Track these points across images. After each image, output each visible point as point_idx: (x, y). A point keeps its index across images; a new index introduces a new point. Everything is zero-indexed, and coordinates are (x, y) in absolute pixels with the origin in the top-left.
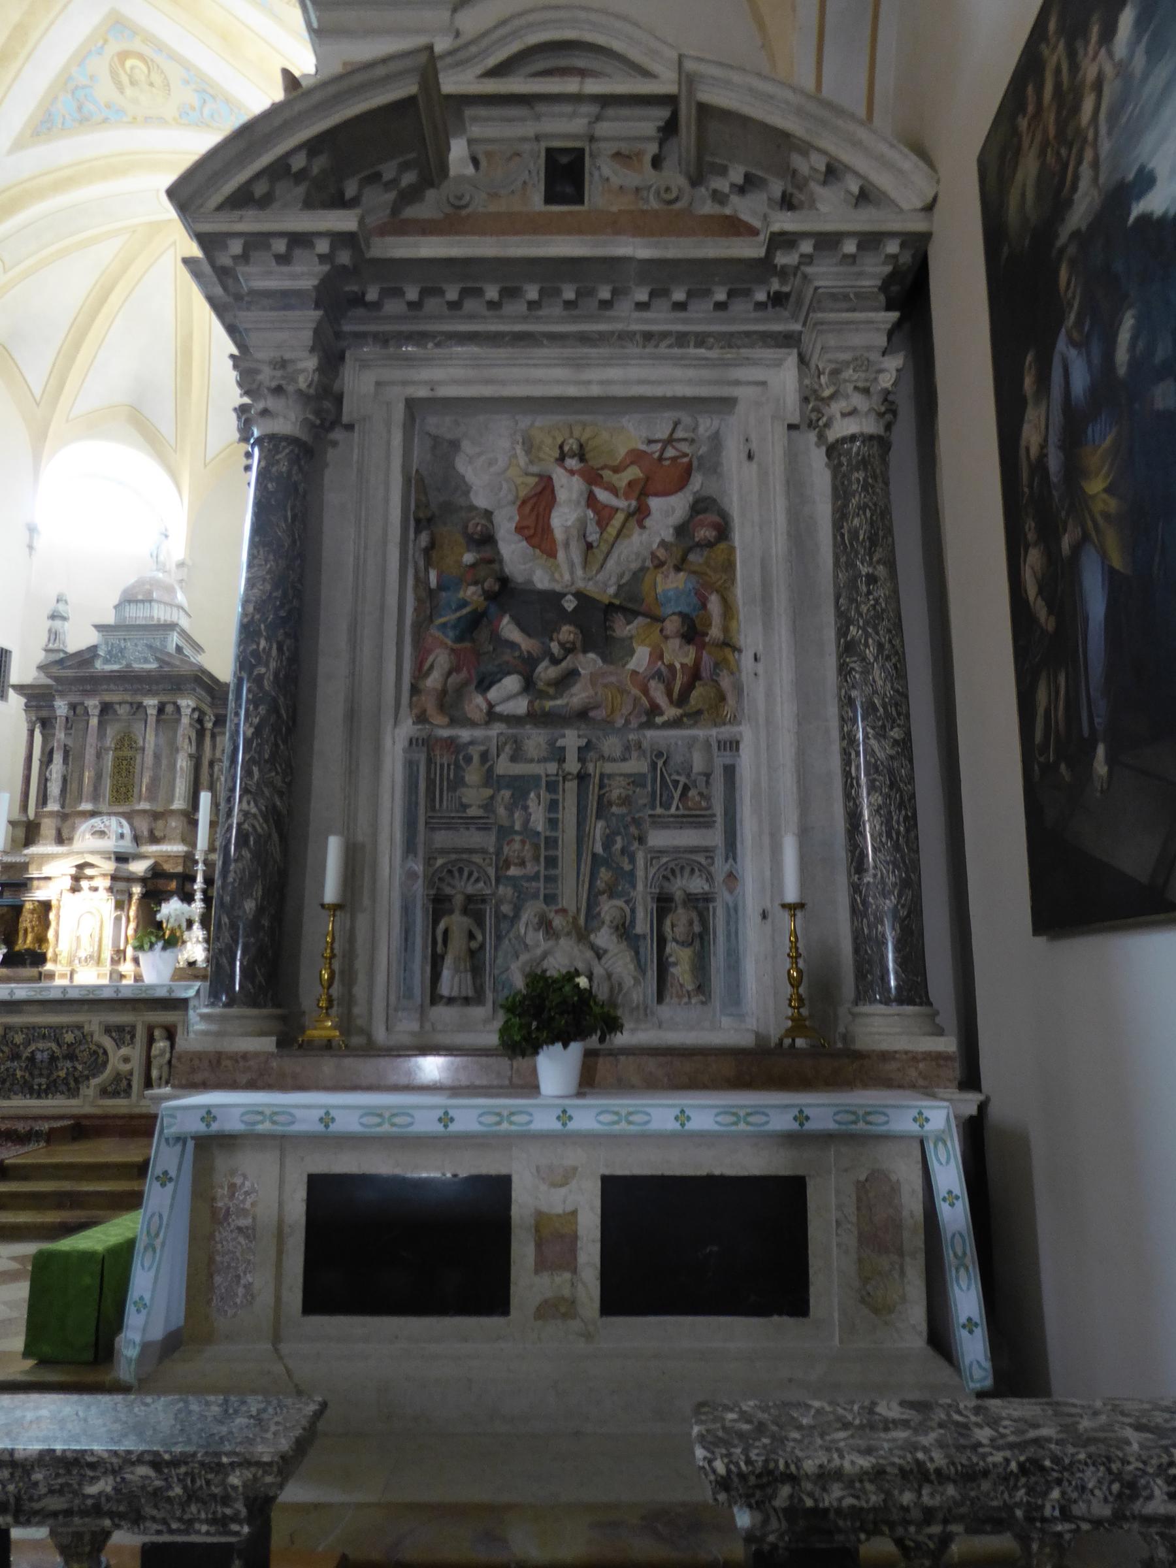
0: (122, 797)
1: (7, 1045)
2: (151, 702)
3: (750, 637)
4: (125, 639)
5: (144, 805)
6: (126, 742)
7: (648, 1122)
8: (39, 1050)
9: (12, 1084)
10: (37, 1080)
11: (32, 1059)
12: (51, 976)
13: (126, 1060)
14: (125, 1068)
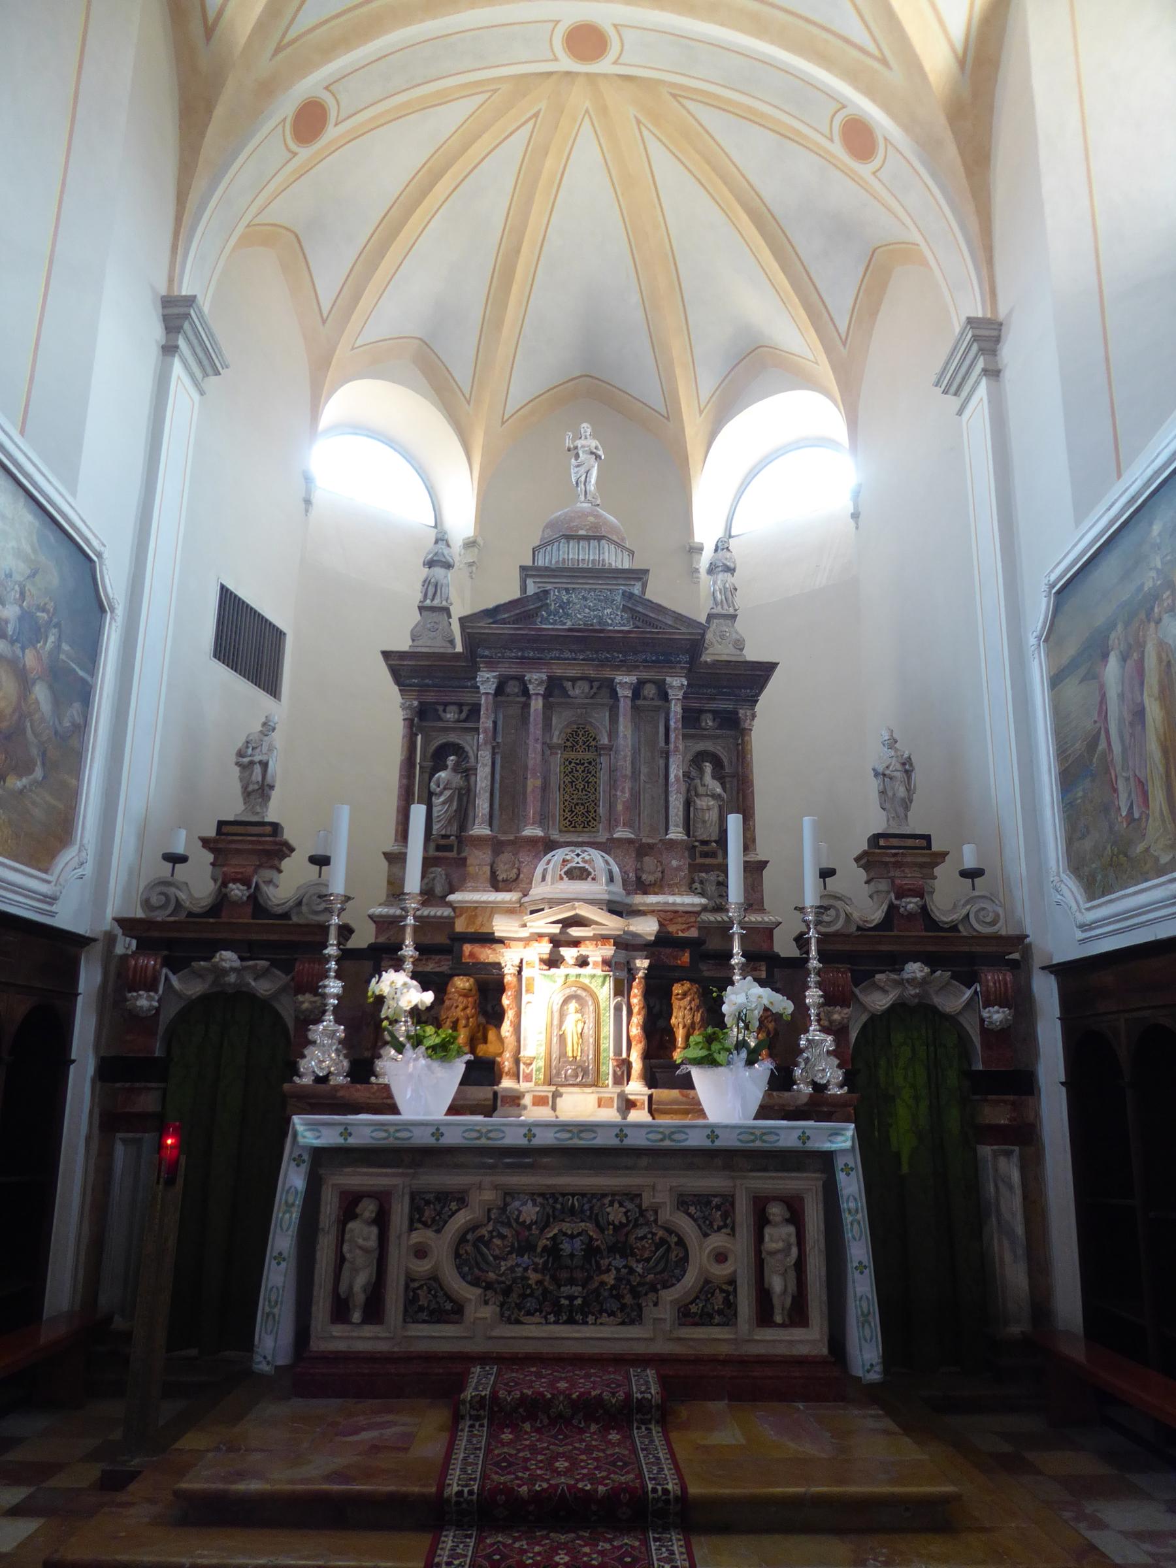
1: (509, 1225)
2: (625, 680)
4: (567, 590)
5: (621, 833)
8: (565, 1234)
9: (523, 1296)
10: (566, 1290)
11: (553, 1250)
12: (515, 1099)
13: (721, 1257)
14: (720, 1271)
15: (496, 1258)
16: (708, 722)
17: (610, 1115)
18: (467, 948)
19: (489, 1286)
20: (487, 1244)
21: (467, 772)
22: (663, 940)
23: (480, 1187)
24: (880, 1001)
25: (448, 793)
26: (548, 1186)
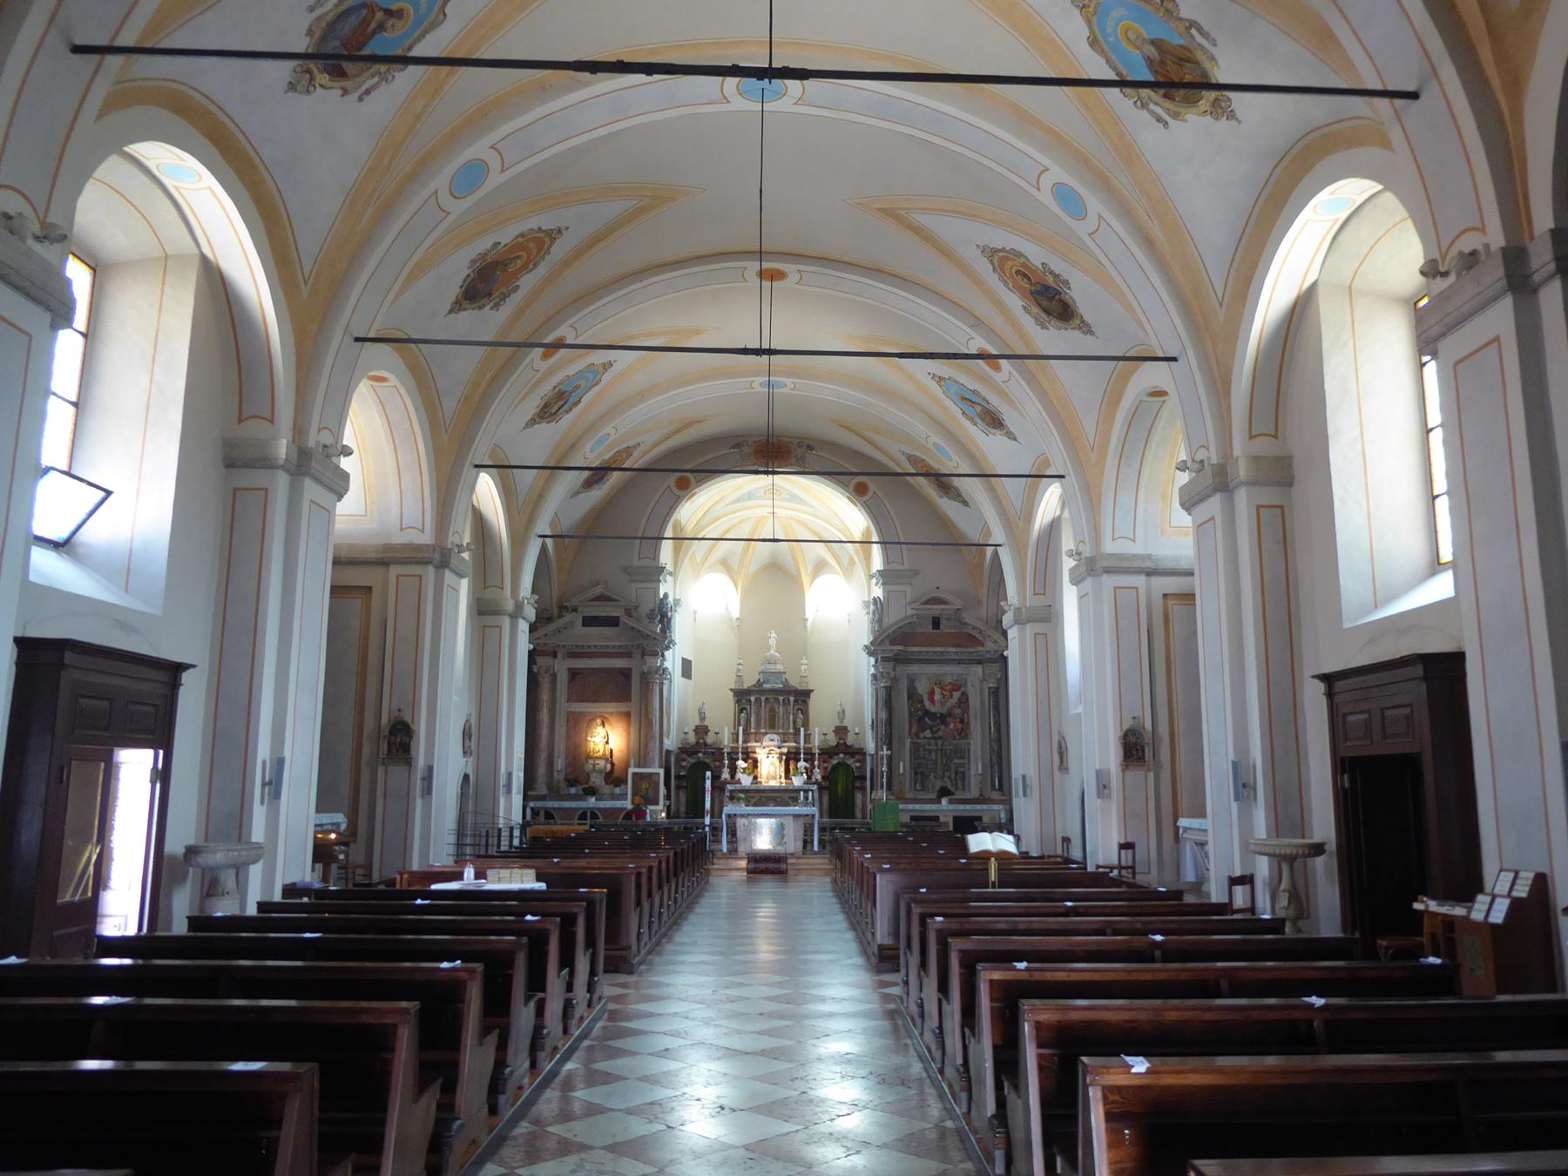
2: (781, 698)
3: (973, 724)
5: (780, 731)
6: (772, 710)
12: (761, 782)
16: (800, 702)
17: (778, 784)
21: (749, 715)
22: (788, 752)
24: (835, 762)
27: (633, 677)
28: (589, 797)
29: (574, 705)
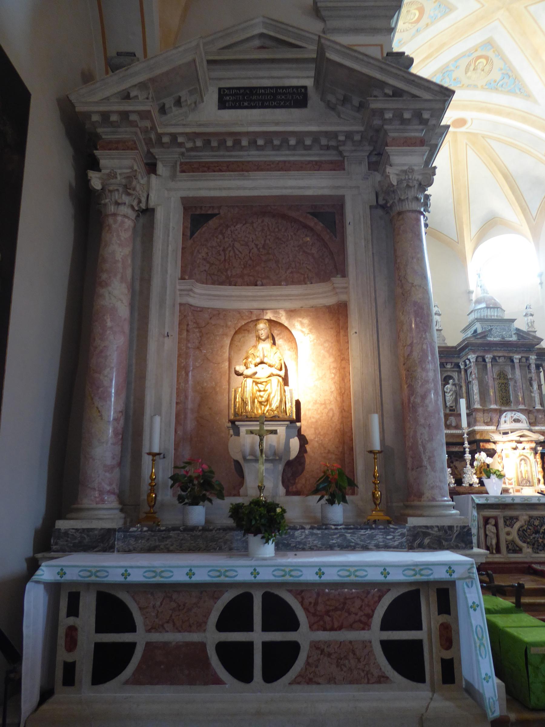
0: (505, 402)
1: (531, 526)
5: (521, 407)
6: (502, 375)
7: (366, 576)
9: (538, 546)
13: (508, 534)
15: (529, 535)
18: (481, 444)
19: (528, 543)
20: (526, 531)
23: (522, 515)
25: (451, 392)
26: (542, 515)
27: (349, 217)
28: (254, 540)
29: (199, 289)
